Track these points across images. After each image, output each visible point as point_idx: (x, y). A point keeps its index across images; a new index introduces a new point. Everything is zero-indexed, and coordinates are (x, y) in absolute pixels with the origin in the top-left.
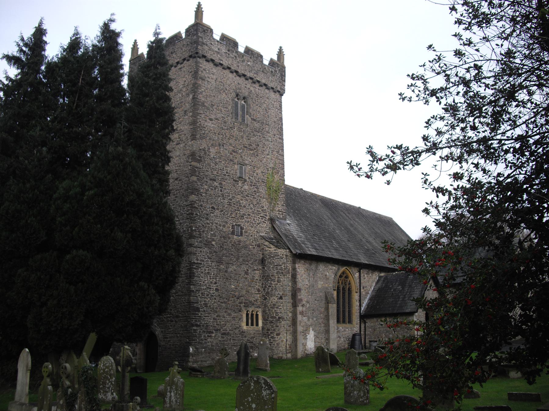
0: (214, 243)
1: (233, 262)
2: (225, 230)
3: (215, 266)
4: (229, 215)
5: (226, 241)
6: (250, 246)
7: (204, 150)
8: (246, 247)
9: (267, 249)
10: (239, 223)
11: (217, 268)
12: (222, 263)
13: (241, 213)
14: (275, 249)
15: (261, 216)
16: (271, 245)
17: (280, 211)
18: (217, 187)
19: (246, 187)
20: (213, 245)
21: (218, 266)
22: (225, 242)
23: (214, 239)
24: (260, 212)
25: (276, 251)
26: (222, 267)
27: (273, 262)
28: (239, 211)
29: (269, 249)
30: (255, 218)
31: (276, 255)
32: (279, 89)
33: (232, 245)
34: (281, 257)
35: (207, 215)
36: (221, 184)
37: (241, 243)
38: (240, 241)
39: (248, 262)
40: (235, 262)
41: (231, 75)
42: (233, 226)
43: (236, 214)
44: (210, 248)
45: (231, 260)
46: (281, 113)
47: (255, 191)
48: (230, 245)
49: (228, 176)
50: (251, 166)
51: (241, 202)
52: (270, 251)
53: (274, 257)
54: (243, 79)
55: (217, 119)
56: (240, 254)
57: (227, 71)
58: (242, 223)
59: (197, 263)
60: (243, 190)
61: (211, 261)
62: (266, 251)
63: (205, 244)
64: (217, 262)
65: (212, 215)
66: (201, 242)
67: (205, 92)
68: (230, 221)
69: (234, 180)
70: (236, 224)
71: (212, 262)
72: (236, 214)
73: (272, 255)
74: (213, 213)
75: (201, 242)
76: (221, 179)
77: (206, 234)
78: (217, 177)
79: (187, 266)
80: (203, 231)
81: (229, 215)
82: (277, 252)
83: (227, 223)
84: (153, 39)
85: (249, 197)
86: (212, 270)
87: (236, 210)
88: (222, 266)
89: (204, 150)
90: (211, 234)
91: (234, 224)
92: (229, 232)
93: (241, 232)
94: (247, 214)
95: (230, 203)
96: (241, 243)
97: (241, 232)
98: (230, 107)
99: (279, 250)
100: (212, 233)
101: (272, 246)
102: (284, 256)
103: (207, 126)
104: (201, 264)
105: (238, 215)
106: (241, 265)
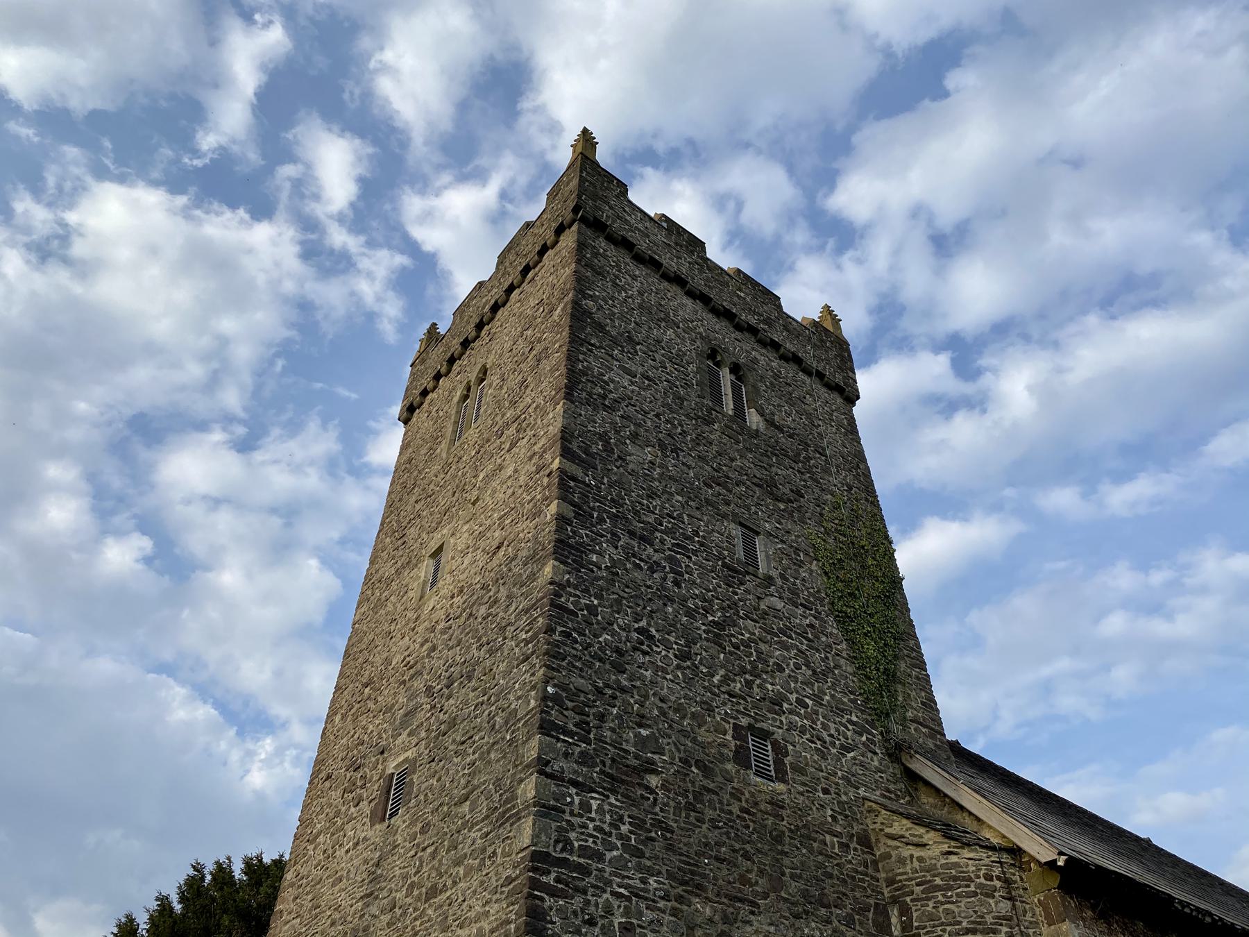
0: (654, 781)
1: (756, 894)
2: (704, 735)
3: (666, 898)
4: (716, 679)
5: (712, 786)
6: (828, 838)
7: (603, 437)
8: (806, 834)
9: (907, 852)
10: (764, 725)
11: (675, 913)
12: (699, 887)
13: (770, 687)
14: (945, 848)
15: (850, 721)
16: (922, 830)
17: (921, 724)
18: (658, 564)
19: (780, 605)
20: (652, 791)
21: (680, 899)
22: (709, 790)
23: (653, 763)
24: (843, 703)
25: (954, 859)
26: (702, 909)
27: (947, 912)
28: (757, 676)
29: (917, 853)
30: (832, 726)
31: (955, 878)
32: (839, 379)
33: (742, 810)
34: (980, 886)
35: (618, 651)
36: (670, 559)
37: (784, 813)
38: (777, 804)
39: (827, 906)
40: (765, 896)
41: (688, 302)
42: (736, 726)
43: (749, 684)
44: (631, 801)
45: (744, 880)
46: (859, 443)
47: (811, 626)
48: (735, 809)
49: (702, 544)
50: (783, 542)
51: (763, 647)
52: (920, 859)
53: (950, 888)
54: (724, 323)
55: (648, 378)
56: (786, 861)
57: (675, 289)
58: (776, 726)
59: (563, 863)
60: (763, 607)
61: (639, 868)
62: (902, 861)
63: (611, 776)
64: (670, 876)
65: (641, 658)
66: (584, 759)
67: (604, 300)
68: (724, 704)
69: (724, 565)
70: (751, 727)
71: (651, 872)
72: (749, 684)
73: (938, 881)
74: (645, 653)
75: (584, 759)
76: (673, 545)
77: (613, 730)
78: (658, 534)
79: (509, 880)
80: (602, 717)
81: (716, 679)
82: (956, 865)
83: (711, 710)
84: (278, 858)
85: (790, 637)
86: (649, 915)
87: (743, 671)
88: (697, 903)
89: (603, 437)
90: (637, 735)
91: (744, 721)
92: (725, 751)
93: (779, 764)
94: (793, 697)
95: (716, 635)
96: (784, 813)
97: (779, 764)
98: (692, 368)
99: (967, 853)
100: (644, 732)
101: (930, 837)
102: (998, 884)
103: (613, 381)
104: (585, 871)
105: (756, 690)
106: (797, 916)
